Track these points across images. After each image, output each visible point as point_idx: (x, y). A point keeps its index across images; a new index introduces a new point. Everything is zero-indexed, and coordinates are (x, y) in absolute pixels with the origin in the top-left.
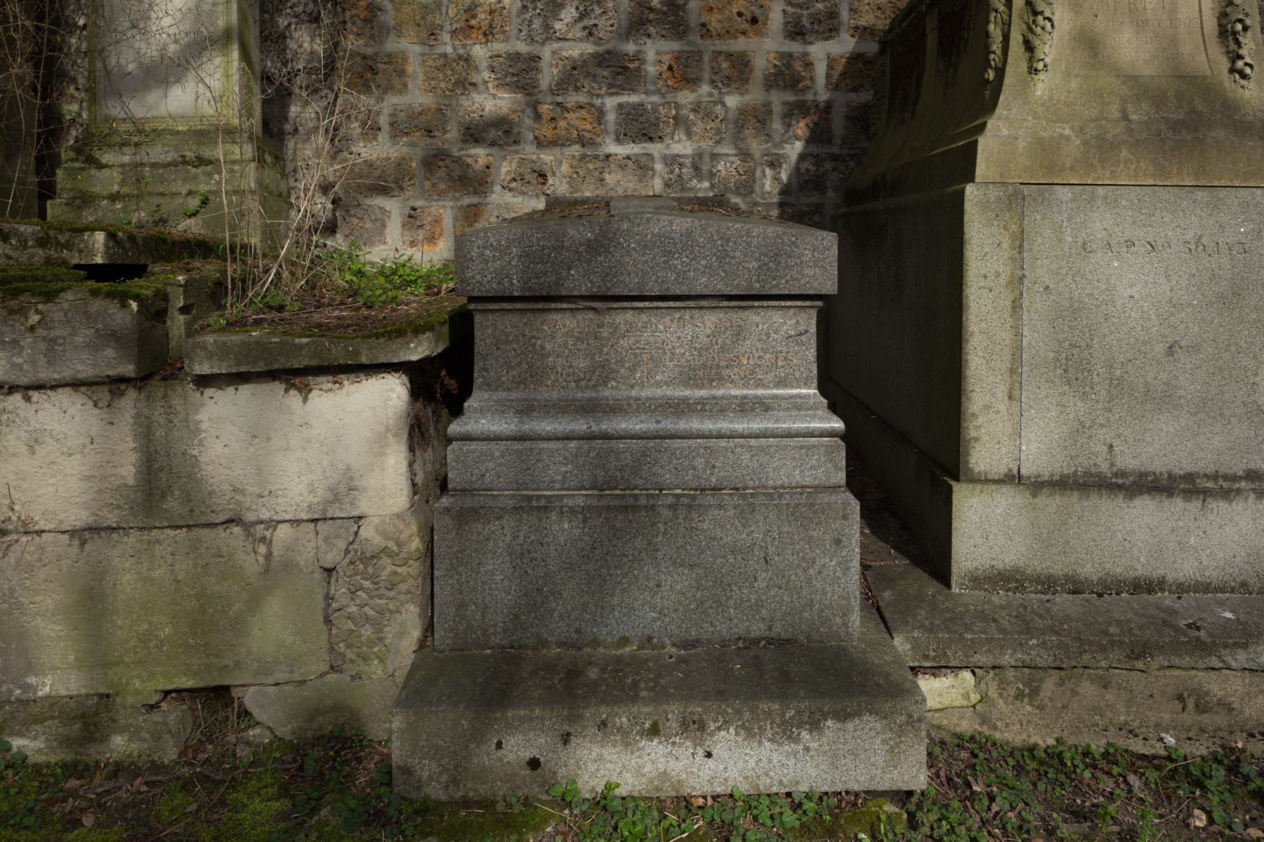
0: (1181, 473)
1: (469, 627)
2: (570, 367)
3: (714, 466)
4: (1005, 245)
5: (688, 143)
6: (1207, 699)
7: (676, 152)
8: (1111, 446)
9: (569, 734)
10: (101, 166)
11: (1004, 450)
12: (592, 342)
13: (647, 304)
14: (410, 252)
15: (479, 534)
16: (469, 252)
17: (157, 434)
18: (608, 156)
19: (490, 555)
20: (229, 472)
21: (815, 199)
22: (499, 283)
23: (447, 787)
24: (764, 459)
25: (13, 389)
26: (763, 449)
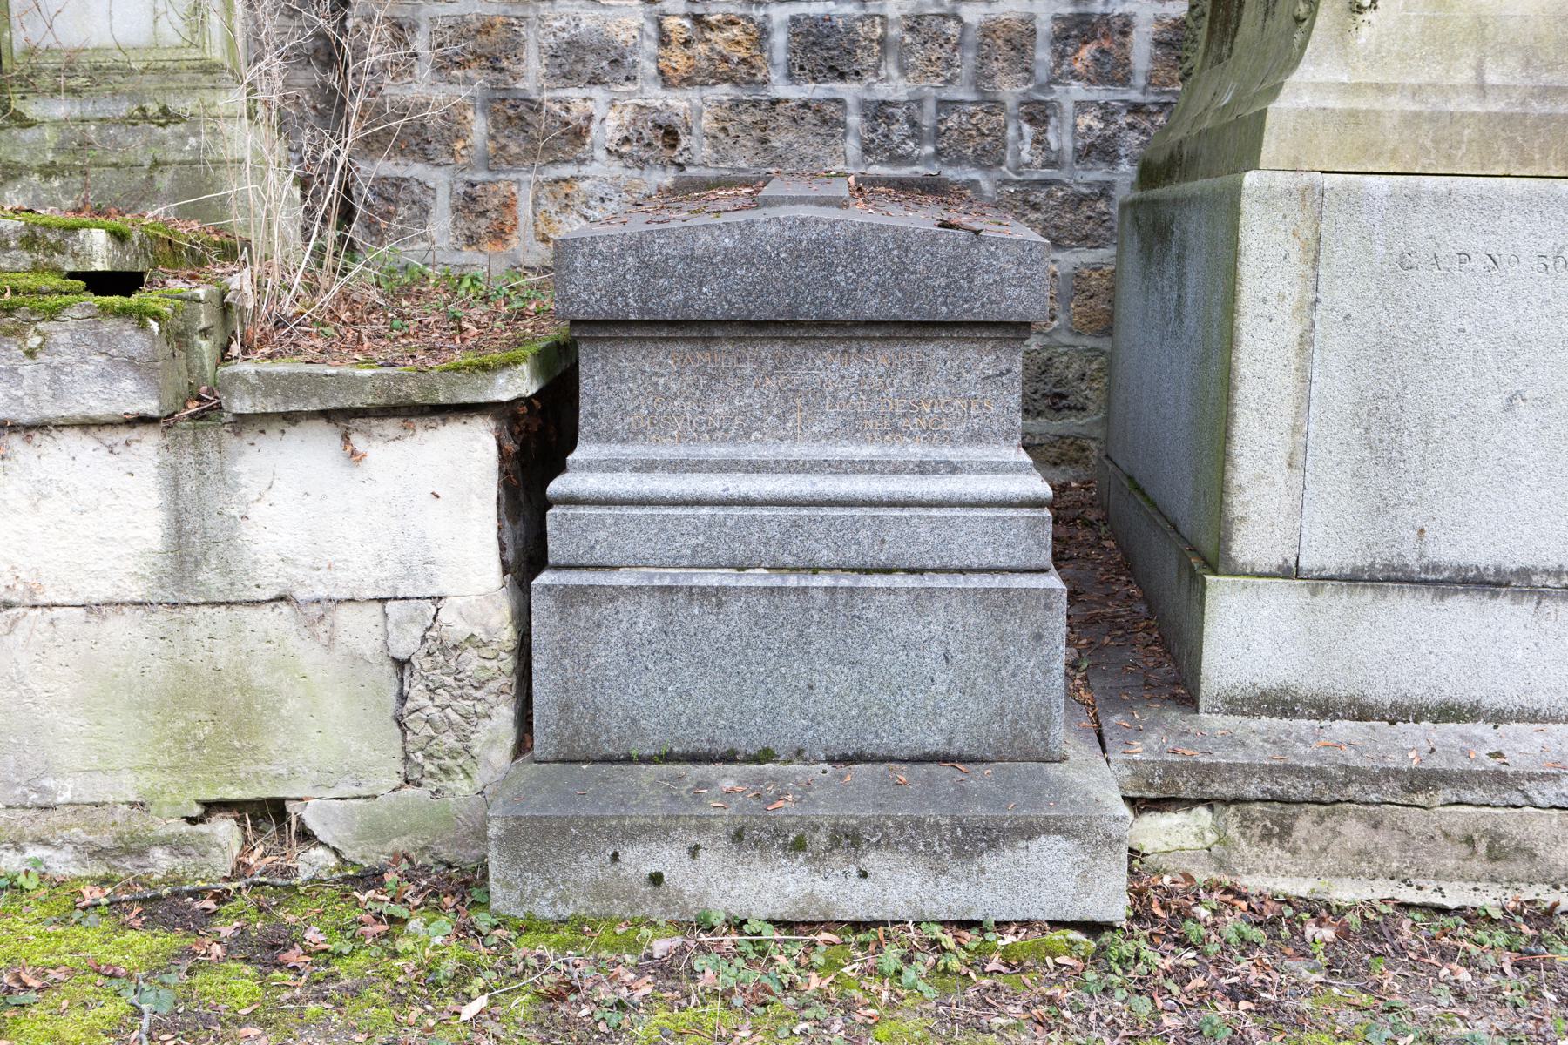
0: (1514, 567)
1: (577, 732)
2: (702, 413)
3: (883, 541)
4: (1294, 258)
5: (902, 82)
6: (1504, 842)
7: (881, 97)
8: (1422, 531)
9: (697, 847)
10: (25, 123)
11: (1278, 534)
12: (730, 381)
13: (801, 332)
14: (467, 255)
15: (588, 619)
16: (572, 262)
17: (187, 488)
18: (774, 102)
19: (601, 646)
20: (276, 537)
21: (1099, 174)
22: (611, 303)
23: (554, 904)
24: (947, 532)
25: (14, 428)
26: (946, 521)
